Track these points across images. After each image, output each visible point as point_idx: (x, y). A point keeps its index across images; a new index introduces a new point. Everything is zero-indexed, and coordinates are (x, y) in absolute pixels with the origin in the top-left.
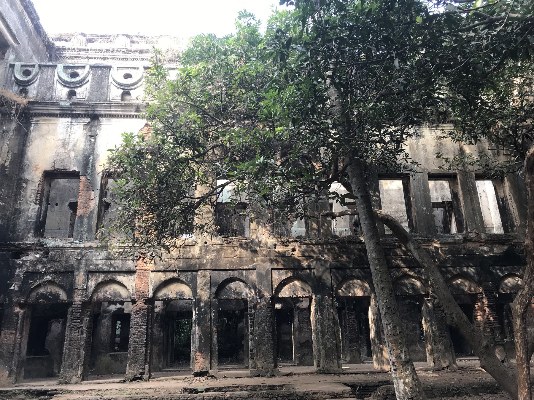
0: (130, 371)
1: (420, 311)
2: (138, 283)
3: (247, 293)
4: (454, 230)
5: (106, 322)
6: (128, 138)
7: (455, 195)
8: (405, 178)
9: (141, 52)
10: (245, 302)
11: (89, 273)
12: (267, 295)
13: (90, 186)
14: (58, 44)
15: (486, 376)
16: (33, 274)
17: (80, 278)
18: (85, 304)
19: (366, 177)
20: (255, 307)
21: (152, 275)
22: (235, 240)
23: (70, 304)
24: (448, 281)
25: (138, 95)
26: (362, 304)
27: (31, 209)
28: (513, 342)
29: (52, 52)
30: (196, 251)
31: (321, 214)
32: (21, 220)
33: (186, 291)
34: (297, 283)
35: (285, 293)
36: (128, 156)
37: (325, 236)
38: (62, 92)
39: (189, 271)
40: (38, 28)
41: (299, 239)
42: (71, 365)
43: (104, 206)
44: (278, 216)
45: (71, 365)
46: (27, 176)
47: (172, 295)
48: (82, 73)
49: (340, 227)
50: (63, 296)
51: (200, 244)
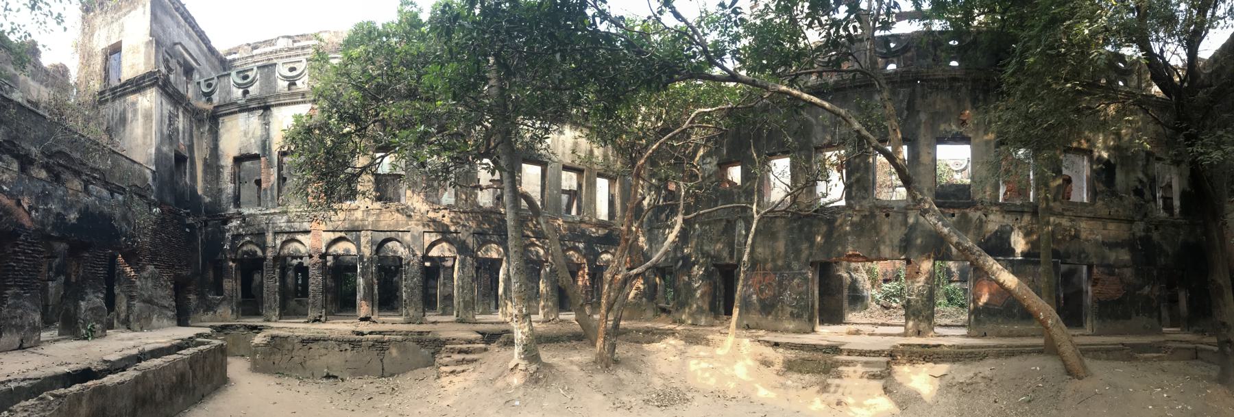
0: (312, 314)
1: (539, 274)
2: (313, 240)
3: (402, 251)
4: (574, 212)
5: (291, 273)
6: (298, 118)
7: (580, 186)
8: (543, 164)
9: (303, 48)
10: (400, 259)
11: (276, 233)
12: (419, 254)
13: (269, 164)
14: (229, 58)
15: (577, 327)
16: (237, 237)
17: (269, 238)
18: (276, 259)
19: (512, 156)
20: (408, 264)
21: (324, 234)
22: (393, 205)
23: (264, 259)
24: (564, 251)
25: (301, 85)
26: (496, 264)
27: (229, 188)
28: (599, 304)
29: (224, 65)
30: (359, 214)
31: (469, 184)
32: (224, 197)
33: (353, 249)
34: (444, 244)
35: (434, 252)
36: (299, 133)
37: (472, 206)
38: (238, 93)
39: (354, 231)
40: (212, 50)
41: (448, 207)
42: (270, 307)
43: (282, 179)
44: (431, 184)
45: (270, 307)
46: (222, 163)
47: (341, 252)
48: (251, 74)
49: (485, 199)
50: (260, 253)
51: (363, 208)
